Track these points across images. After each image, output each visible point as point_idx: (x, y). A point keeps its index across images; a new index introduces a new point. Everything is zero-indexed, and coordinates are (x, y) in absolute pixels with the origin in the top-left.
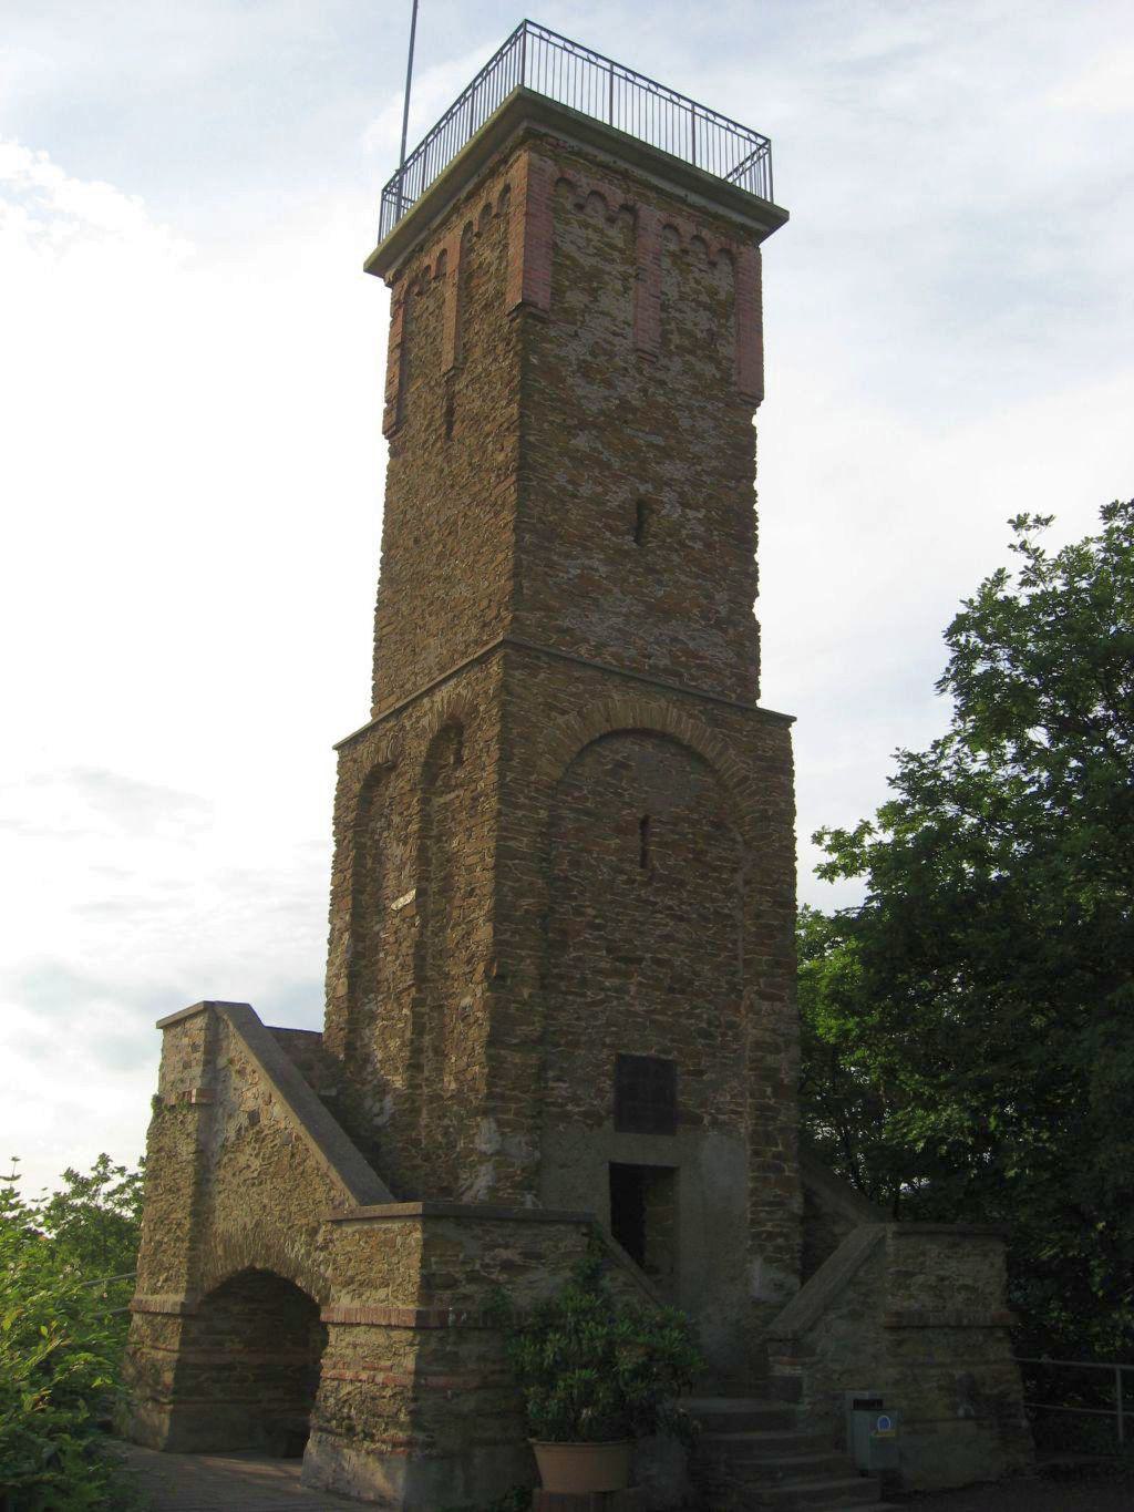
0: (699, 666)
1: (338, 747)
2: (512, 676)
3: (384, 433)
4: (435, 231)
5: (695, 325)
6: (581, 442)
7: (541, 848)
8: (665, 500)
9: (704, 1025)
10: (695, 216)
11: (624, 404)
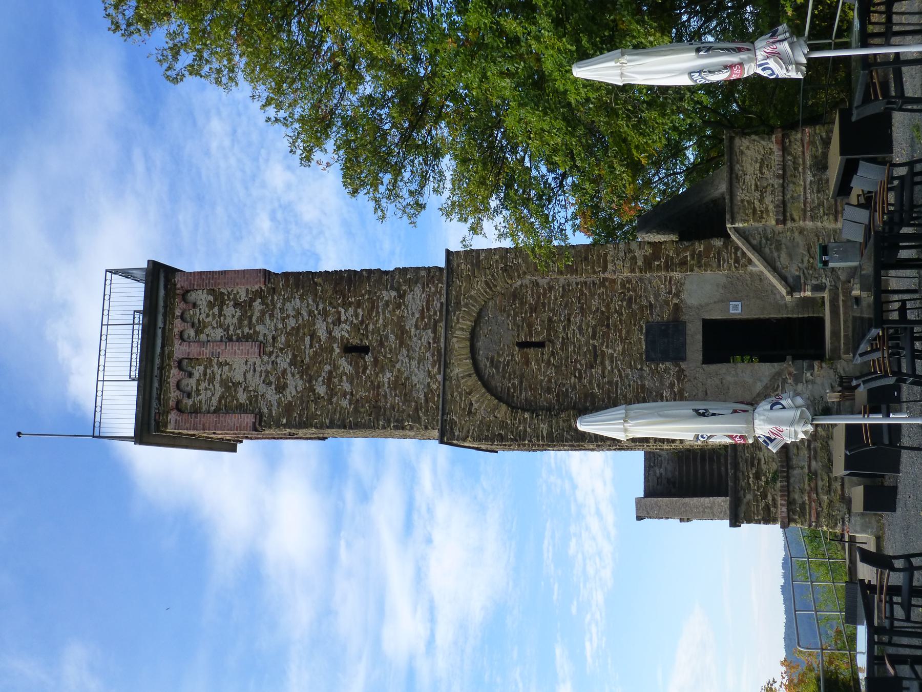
0: (428, 310)
2: (458, 436)
5: (233, 316)
6: (321, 390)
7: (545, 416)
9: (625, 303)
10: (169, 321)
11: (293, 363)
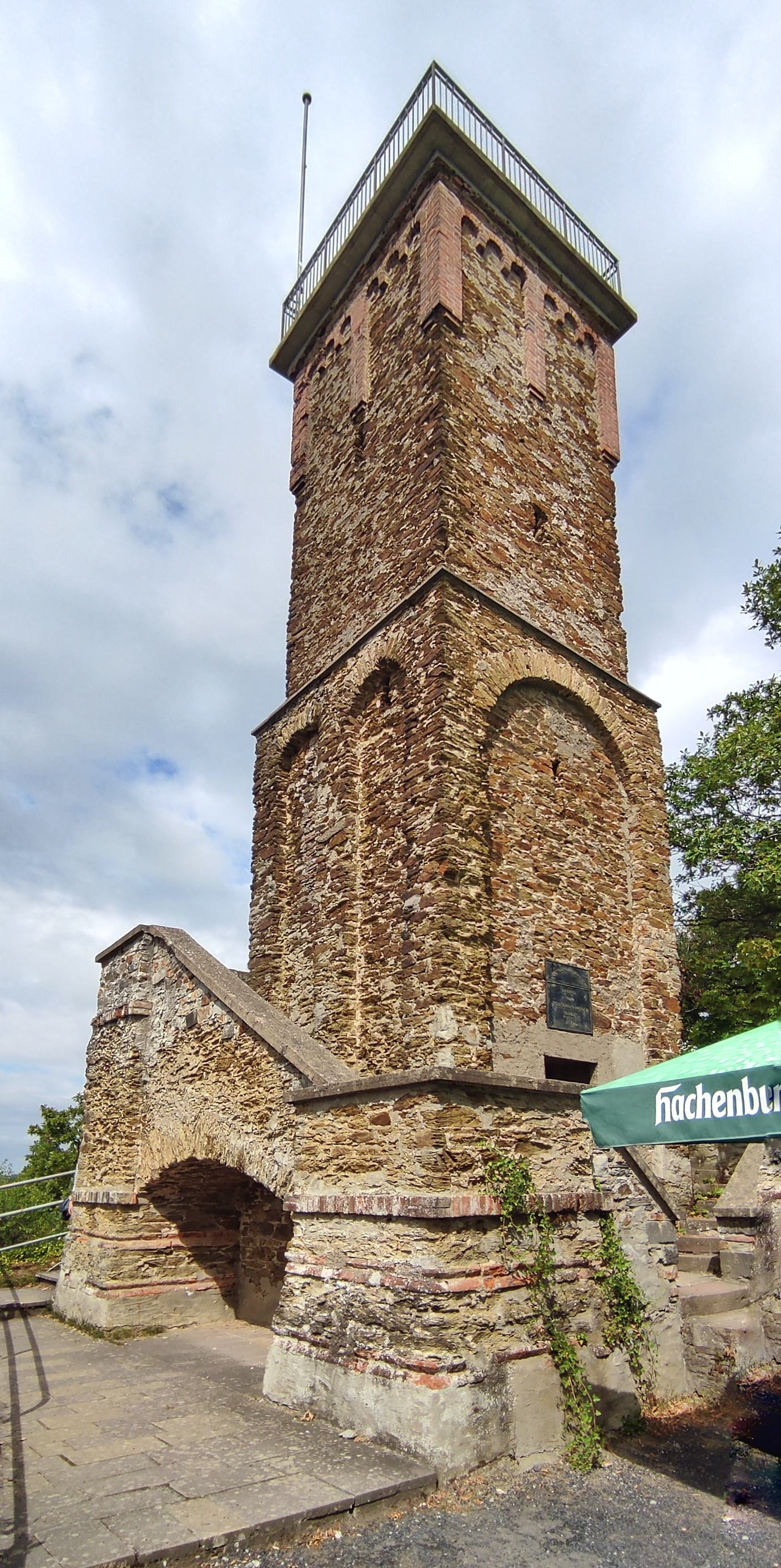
3: (291, 489)
4: (338, 307)
6: (491, 441)
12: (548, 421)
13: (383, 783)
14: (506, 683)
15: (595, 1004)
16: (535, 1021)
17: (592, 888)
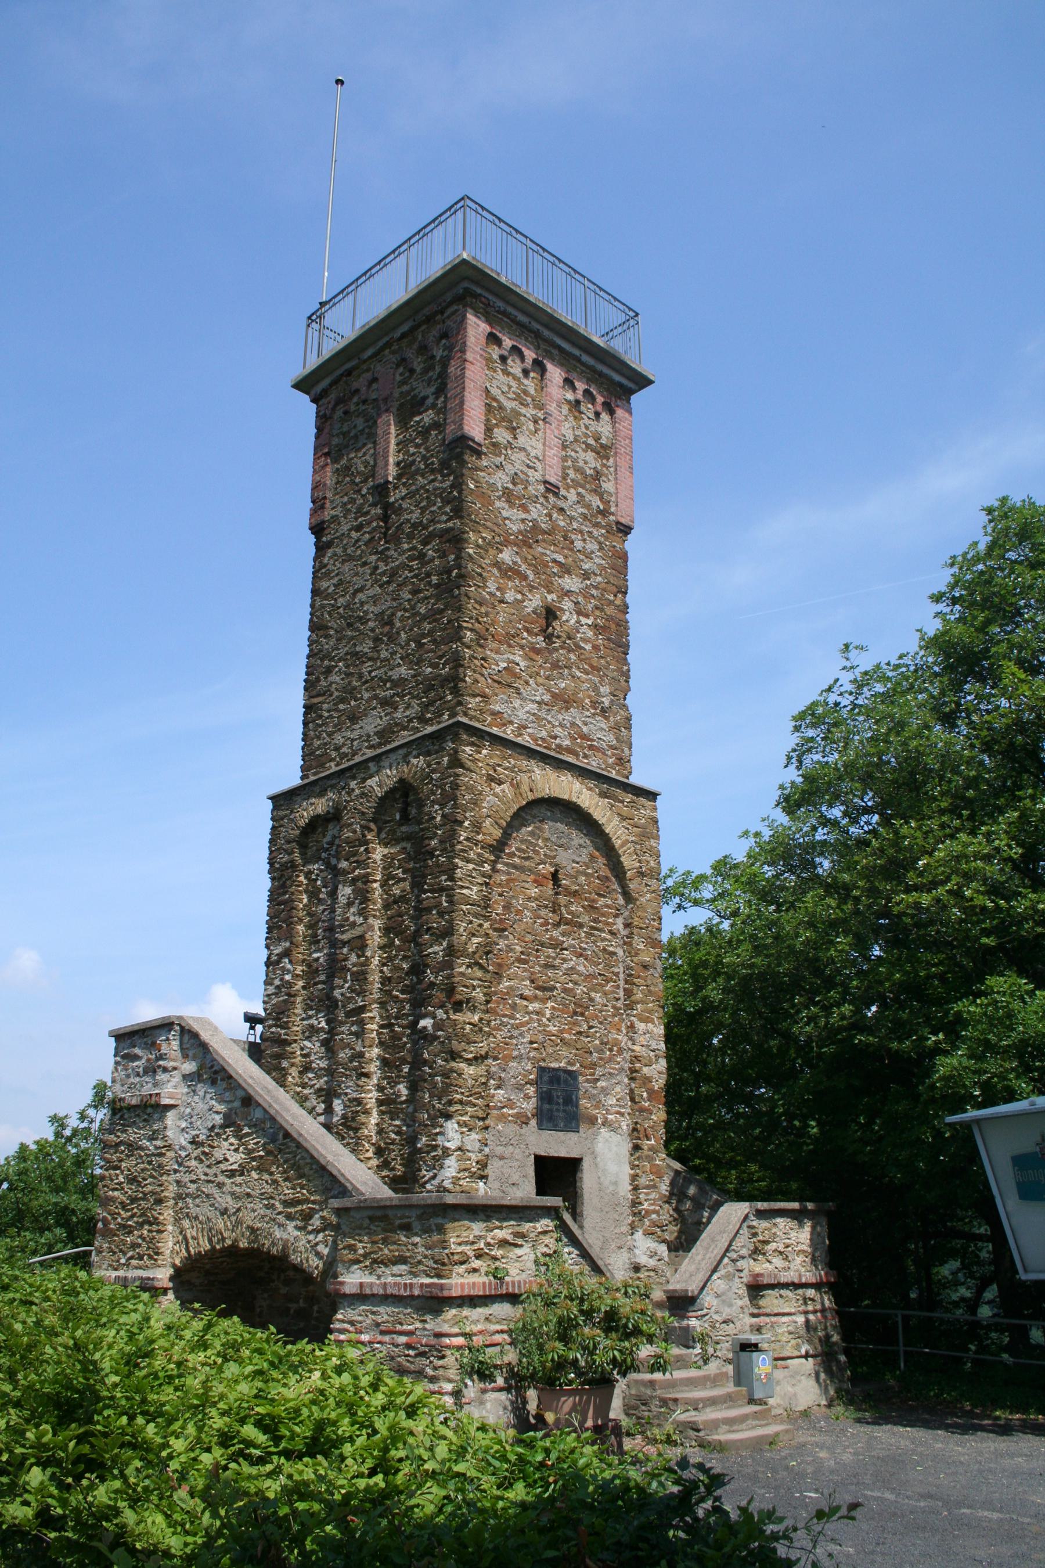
0: (591, 747)
1: (272, 798)
3: (310, 529)
4: (365, 361)
6: (506, 556)
8: (566, 608)
11: (535, 528)
12: (562, 510)
13: (401, 897)
14: (510, 813)
15: (583, 1102)
16: (527, 1124)
17: (585, 989)
